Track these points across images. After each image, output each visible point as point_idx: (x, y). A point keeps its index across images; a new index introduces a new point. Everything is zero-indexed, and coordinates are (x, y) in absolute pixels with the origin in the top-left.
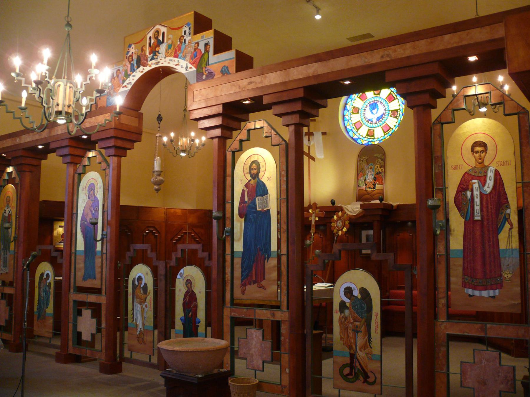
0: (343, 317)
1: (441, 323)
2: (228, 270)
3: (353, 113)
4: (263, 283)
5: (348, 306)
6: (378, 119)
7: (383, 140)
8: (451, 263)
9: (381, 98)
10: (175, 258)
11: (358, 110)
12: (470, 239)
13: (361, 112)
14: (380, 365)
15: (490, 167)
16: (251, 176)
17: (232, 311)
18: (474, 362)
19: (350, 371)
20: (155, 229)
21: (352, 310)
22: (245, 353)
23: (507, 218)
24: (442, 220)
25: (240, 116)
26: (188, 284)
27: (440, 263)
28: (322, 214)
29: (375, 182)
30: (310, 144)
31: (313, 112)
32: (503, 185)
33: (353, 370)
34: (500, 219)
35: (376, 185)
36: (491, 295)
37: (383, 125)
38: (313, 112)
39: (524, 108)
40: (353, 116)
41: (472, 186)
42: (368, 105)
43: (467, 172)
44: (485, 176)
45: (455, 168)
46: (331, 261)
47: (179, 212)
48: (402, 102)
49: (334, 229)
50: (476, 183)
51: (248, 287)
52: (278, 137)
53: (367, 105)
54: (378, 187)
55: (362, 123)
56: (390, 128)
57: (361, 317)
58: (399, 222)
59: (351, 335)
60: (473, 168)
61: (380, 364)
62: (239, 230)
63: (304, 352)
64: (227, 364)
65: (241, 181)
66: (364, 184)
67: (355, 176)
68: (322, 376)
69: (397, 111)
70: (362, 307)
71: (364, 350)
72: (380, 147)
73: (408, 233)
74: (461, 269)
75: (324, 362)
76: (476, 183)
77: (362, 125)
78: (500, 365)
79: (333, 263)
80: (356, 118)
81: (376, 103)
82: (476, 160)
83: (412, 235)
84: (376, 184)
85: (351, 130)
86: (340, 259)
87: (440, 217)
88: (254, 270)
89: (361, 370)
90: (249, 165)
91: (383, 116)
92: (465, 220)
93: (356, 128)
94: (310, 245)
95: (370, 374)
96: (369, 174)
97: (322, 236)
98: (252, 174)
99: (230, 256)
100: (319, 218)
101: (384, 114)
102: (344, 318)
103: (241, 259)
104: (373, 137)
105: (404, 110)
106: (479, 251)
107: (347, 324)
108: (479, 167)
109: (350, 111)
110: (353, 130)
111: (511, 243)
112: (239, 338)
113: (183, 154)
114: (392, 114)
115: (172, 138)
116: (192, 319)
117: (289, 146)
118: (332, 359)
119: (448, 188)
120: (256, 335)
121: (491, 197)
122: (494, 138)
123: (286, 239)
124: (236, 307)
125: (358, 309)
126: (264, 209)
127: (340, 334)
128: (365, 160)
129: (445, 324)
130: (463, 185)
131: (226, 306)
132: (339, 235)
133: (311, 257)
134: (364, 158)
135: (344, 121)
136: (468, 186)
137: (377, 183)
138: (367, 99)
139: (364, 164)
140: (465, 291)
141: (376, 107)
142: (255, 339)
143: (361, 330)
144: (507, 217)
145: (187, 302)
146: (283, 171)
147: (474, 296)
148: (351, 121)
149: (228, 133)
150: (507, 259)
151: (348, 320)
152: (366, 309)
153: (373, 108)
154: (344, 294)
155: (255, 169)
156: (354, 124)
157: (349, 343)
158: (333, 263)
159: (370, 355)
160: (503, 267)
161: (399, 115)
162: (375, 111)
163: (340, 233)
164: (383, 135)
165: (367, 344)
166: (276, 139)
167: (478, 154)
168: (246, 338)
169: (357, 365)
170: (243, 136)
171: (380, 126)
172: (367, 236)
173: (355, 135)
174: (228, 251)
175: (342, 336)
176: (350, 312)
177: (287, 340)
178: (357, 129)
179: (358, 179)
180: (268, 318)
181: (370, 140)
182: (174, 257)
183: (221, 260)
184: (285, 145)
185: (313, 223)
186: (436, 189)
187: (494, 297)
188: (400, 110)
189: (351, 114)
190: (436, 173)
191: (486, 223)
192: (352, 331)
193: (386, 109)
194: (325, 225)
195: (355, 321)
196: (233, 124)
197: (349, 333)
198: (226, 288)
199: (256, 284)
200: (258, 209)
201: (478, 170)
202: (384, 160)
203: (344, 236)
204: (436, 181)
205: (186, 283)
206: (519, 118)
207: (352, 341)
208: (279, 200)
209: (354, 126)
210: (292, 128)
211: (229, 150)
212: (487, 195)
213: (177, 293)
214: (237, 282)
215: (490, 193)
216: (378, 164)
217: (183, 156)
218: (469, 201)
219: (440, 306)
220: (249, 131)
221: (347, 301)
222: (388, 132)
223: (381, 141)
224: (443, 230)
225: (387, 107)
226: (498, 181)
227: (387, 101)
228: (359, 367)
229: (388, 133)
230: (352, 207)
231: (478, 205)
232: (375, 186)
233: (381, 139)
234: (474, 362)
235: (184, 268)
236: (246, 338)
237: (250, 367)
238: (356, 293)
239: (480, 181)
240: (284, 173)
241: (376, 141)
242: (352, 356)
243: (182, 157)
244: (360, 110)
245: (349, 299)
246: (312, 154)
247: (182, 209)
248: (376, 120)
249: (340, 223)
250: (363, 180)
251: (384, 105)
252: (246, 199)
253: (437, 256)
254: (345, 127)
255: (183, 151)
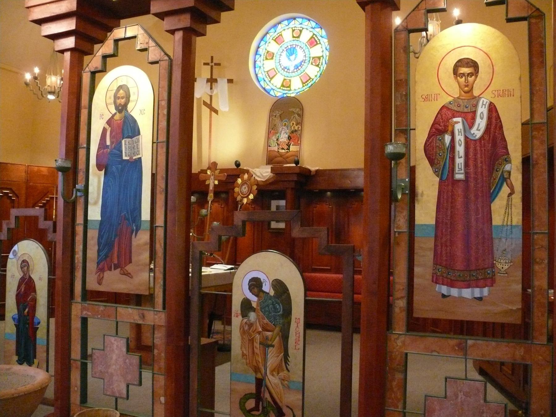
0: (246, 323)
1: (396, 336)
2: (79, 247)
3: (267, 59)
4: (129, 268)
5: (255, 307)
6: (297, 67)
7: (301, 92)
8: (416, 245)
9: (300, 42)
10: (6, 229)
11: (272, 55)
12: (447, 209)
13: (276, 58)
14: (300, 397)
15: (482, 99)
16: (117, 108)
17: (83, 309)
18: (446, 397)
19: (256, 404)
20: (13, 192)
21: (261, 313)
22: (101, 372)
23: (505, 178)
24: (404, 178)
25: (105, 21)
26: (24, 267)
27: (398, 244)
28: (223, 177)
29: (289, 143)
30: (213, 93)
31: (213, 14)
32: (501, 127)
33: (261, 403)
34: (495, 179)
35: (291, 146)
36: (476, 296)
37: (302, 74)
38: (213, 14)
39: (538, 9)
40: (266, 62)
41: (453, 126)
42: (285, 50)
43: (446, 105)
44: (475, 113)
45: (427, 99)
46: (232, 238)
47: (45, 171)
48: (326, 48)
49: (238, 195)
50: (459, 122)
51: (108, 275)
52: (158, 50)
53: (283, 50)
54: (293, 148)
55: (276, 71)
56: (310, 78)
57: (273, 325)
58: (317, 191)
59: (257, 351)
60: (455, 100)
61: (301, 395)
62: (96, 189)
63: (187, 378)
64: (76, 386)
65: (102, 116)
66: (277, 144)
67: (266, 130)
68: (214, 409)
69: (319, 58)
70: (275, 308)
71: (278, 373)
72: (298, 100)
73: (327, 205)
74: (430, 255)
75: (218, 369)
76: (459, 122)
77: (277, 74)
78: (485, 402)
79: (236, 239)
80: (269, 65)
81: (294, 48)
82: (460, 87)
83: (332, 207)
84: (290, 145)
85: (264, 79)
86: (244, 235)
87: (402, 175)
88: (116, 248)
89: (272, 403)
90: (114, 91)
91: (303, 63)
92: (441, 179)
93: (269, 77)
94: (207, 215)
95: (285, 410)
96: (283, 132)
97: (223, 206)
98: (118, 104)
99: (82, 226)
100: (219, 181)
101: (304, 61)
102: (249, 325)
103: (98, 231)
104: (289, 89)
105: (327, 57)
106: (460, 227)
107: (253, 334)
108: (463, 98)
109: (262, 57)
110: (266, 79)
111: (510, 216)
112: (92, 349)
113: (51, 97)
114: (313, 61)
115: (35, 74)
116: (28, 318)
117: (174, 62)
118: (229, 363)
119: (415, 129)
120: (117, 346)
121: (481, 144)
122: (488, 53)
123: (164, 203)
124: (91, 302)
125: (270, 313)
126: (132, 157)
127: (241, 348)
128: (278, 115)
129: (402, 338)
130: (439, 125)
131: (75, 301)
132: (243, 203)
133: (207, 231)
134: (278, 113)
135: (255, 67)
136: (446, 126)
137: (292, 143)
138: (284, 42)
139: (277, 121)
140: (437, 289)
141: (295, 52)
142: (116, 352)
143: (273, 344)
144: (505, 177)
145: (22, 293)
146: (164, 100)
147: (450, 296)
148: (264, 68)
149: (85, 46)
150: (504, 240)
151: (254, 329)
152: (281, 313)
153: (290, 54)
154: (249, 289)
155: (122, 98)
156: (267, 72)
157: (255, 364)
158: (236, 239)
159: (286, 382)
160: (497, 254)
161: (322, 63)
162: (292, 58)
163: (245, 201)
164: (302, 86)
165: (282, 363)
166: (154, 54)
167: (464, 78)
168: (104, 350)
169: (267, 396)
170: (107, 49)
171: (299, 75)
172: (278, 207)
173: (268, 85)
174: (80, 220)
175: (245, 352)
176: (258, 316)
177: (163, 355)
178: (270, 78)
179: (269, 138)
180: (134, 320)
181: (286, 92)
182: (5, 228)
183: (70, 233)
184: (167, 62)
185: (211, 188)
186: (396, 130)
187: (480, 299)
188: (323, 58)
189: (263, 60)
190: (396, 106)
191: (472, 185)
192: (260, 344)
193: (306, 56)
194: (227, 193)
195: (265, 329)
196: (95, 32)
197: (256, 347)
198: (76, 274)
199: (119, 269)
200: (125, 158)
201: (463, 103)
202: (301, 116)
203: (250, 206)
204: (396, 119)
205: (21, 264)
206: (529, 25)
207: (260, 360)
208: (155, 145)
209: (267, 75)
210: (179, 35)
211: (87, 69)
212: (475, 140)
213: (9, 279)
214: (92, 266)
215: (482, 138)
216: (294, 120)
217: (51, 100)
218: (448, 149)
219: (397, 310)
220: (116, 41)
221: (254, 299)
222: (308, 82)
223: (299, 94)
224: (406, 194)
225: (307, 53)
226: (494, 120)
227: (308, 45)
228: (269, 399)
229: (308, 84)
230: (261, 171)
231: (461, 157)
232: (289, 147)
233: (299, 90)
234: (446, 397)
235: (18, 244)
236: (104, 350)
237: (108, 393)
238: (267, 288)
239: (466, 121)
240: (164, 103)
241: (293, 93)
242: (260, 383)
243: (50, 101)
244: (275, 56)
245: (256, 296)
246: (214, 105)
247: (49, 167)
248: (293, 68)
249: (245, 188)
250: (276, 139)
251: (304, 51)
252: (108, 143)
253: (395, 235)
254: (257, 75)
255: (50, 93)
